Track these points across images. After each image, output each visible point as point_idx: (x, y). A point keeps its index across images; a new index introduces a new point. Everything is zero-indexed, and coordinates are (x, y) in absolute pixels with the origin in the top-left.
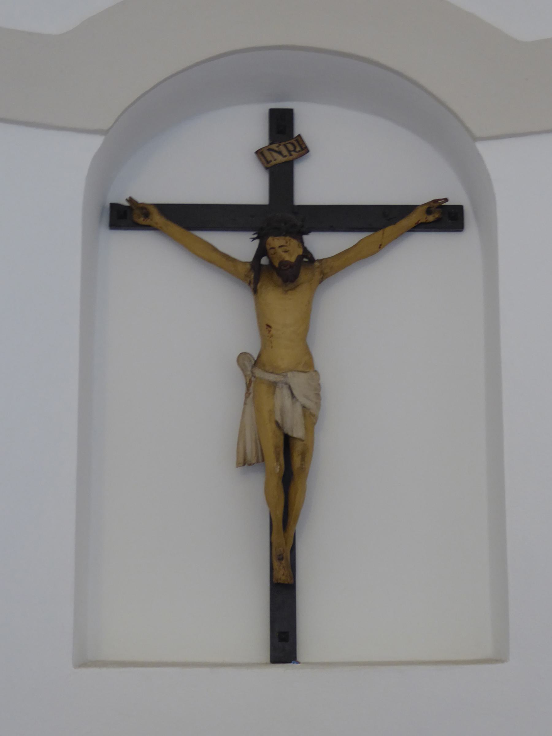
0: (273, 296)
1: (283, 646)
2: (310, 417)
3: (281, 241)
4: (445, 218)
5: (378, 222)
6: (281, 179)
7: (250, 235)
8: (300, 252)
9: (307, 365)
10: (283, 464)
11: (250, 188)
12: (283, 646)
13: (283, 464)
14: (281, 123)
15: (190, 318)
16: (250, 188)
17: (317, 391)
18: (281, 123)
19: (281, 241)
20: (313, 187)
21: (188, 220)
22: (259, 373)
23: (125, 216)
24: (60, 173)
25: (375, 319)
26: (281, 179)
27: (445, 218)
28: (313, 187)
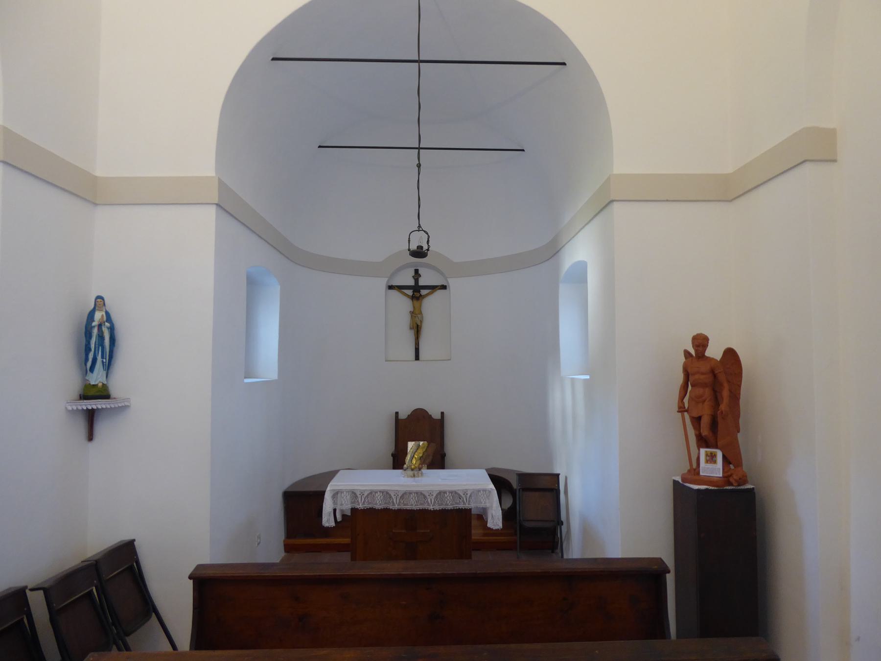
0: (415, 302)
1: (417, 358)
2: (421, 322)
3: (417, 292)
4: (444, 287)
5: (433, 288)
6: (417, 281)
7: (405, 417)
8: (42, 592)
9: (421, 313)
10: (417, 329)
11: (411, 282)
12: (417, 358)
13: (417, 329)
14: (417, 271)
15: (402, 304)
16: (411, 282)
17: (422, 317)
18: (417, 271)
19: (417, 292)
20: (422, 282)
21: (400, 288)
22: (413, 314)
23: (391, 287)
24: (383, 283)
25: (431, 304)
26: (417, 281)
27: (444, 287)
28: (422, 282)
